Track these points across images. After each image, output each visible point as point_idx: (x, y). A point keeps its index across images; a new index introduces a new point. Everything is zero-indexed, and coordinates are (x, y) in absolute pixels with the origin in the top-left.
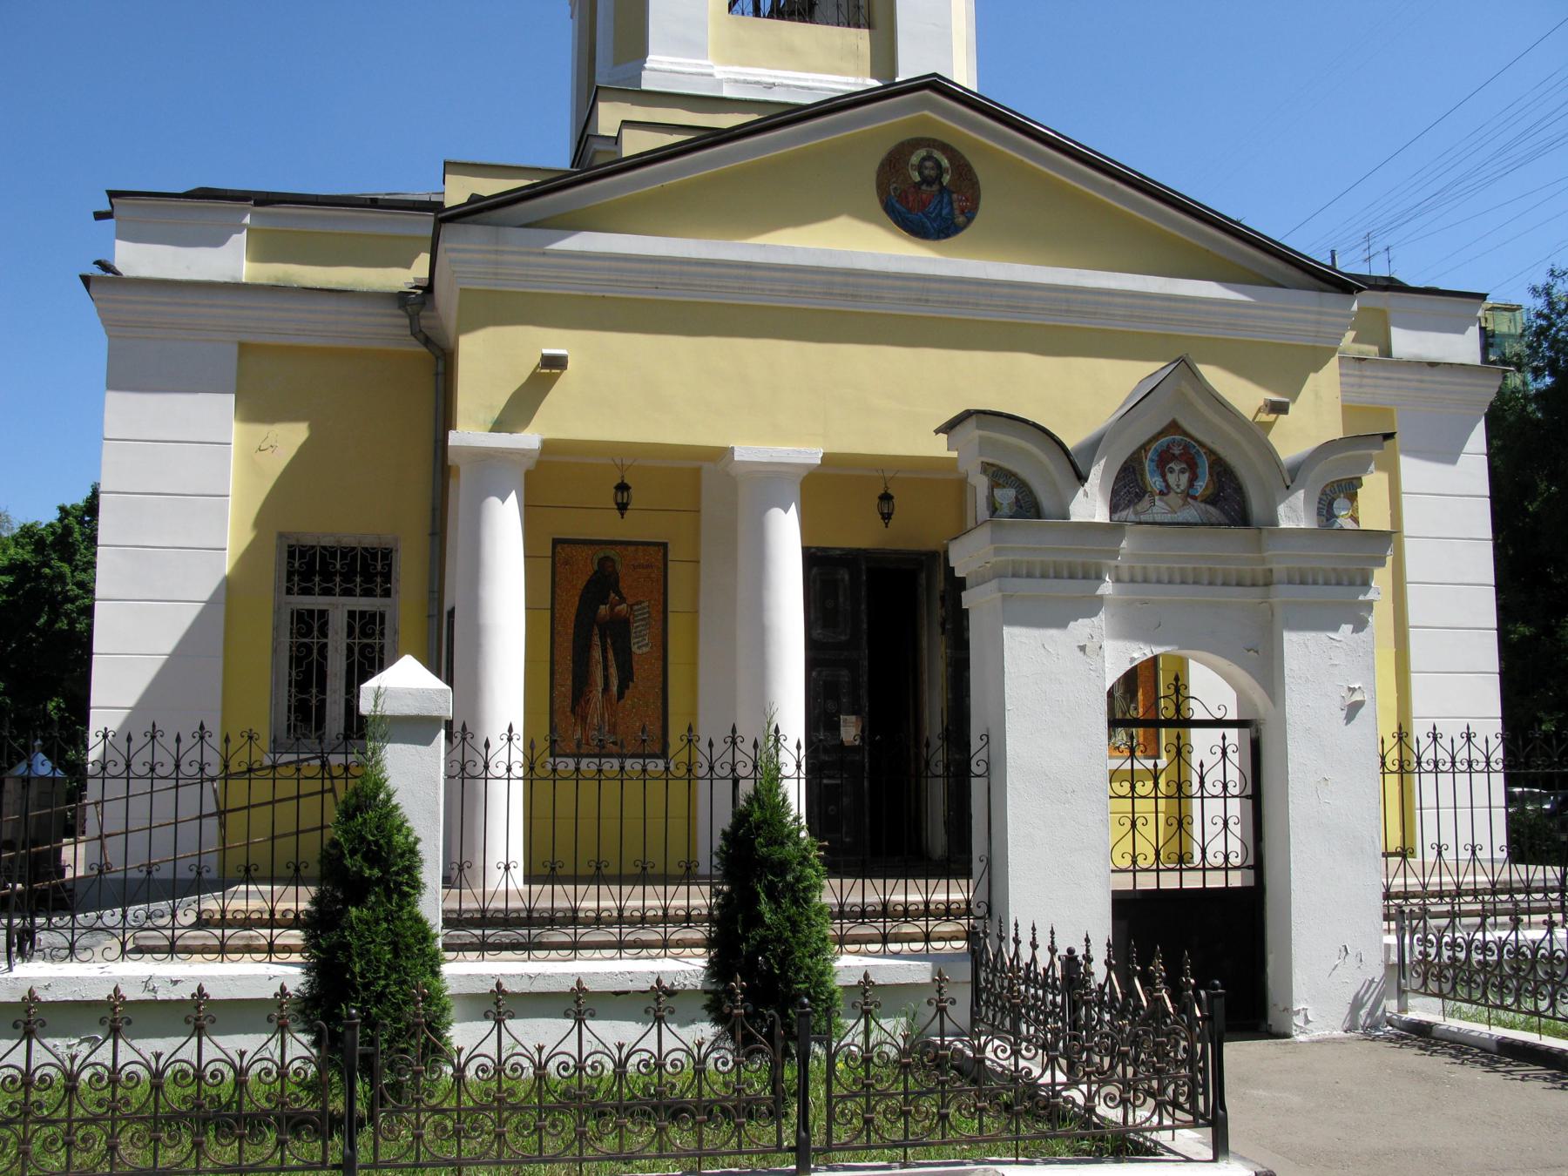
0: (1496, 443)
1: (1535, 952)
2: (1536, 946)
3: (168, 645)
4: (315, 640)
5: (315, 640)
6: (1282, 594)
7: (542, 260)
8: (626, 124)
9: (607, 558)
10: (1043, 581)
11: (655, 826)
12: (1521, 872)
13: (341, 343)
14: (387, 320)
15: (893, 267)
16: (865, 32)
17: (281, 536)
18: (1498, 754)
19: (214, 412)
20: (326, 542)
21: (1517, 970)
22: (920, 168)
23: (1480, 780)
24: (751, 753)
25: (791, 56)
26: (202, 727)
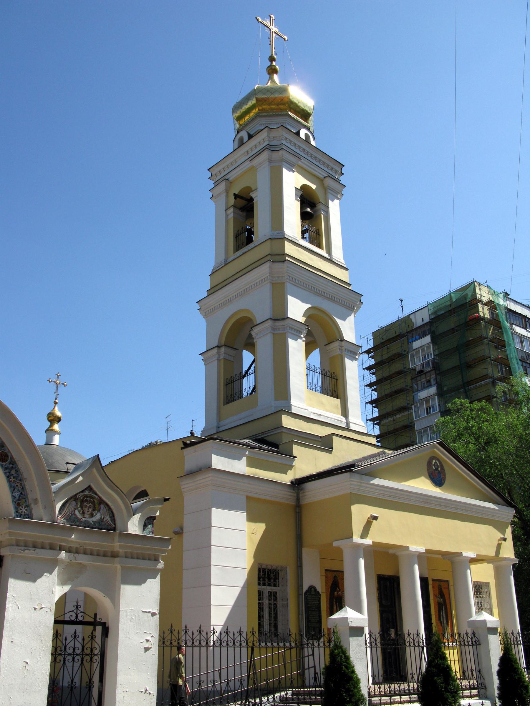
0: (517, 549)
3: (232, 602)
4: (272, 602)
7: (368, 486)
8: (333, 434)
10: (131, 560)
12: (385, 688)
13: (273, 499)
14: (290, 493)
15: (436, 495)
17: (258, 564)
18: (379, 640)
20: (269, 567)
22: (434, 465)
23: (451, 651)
25: (322, 405)
26: (75, 633)
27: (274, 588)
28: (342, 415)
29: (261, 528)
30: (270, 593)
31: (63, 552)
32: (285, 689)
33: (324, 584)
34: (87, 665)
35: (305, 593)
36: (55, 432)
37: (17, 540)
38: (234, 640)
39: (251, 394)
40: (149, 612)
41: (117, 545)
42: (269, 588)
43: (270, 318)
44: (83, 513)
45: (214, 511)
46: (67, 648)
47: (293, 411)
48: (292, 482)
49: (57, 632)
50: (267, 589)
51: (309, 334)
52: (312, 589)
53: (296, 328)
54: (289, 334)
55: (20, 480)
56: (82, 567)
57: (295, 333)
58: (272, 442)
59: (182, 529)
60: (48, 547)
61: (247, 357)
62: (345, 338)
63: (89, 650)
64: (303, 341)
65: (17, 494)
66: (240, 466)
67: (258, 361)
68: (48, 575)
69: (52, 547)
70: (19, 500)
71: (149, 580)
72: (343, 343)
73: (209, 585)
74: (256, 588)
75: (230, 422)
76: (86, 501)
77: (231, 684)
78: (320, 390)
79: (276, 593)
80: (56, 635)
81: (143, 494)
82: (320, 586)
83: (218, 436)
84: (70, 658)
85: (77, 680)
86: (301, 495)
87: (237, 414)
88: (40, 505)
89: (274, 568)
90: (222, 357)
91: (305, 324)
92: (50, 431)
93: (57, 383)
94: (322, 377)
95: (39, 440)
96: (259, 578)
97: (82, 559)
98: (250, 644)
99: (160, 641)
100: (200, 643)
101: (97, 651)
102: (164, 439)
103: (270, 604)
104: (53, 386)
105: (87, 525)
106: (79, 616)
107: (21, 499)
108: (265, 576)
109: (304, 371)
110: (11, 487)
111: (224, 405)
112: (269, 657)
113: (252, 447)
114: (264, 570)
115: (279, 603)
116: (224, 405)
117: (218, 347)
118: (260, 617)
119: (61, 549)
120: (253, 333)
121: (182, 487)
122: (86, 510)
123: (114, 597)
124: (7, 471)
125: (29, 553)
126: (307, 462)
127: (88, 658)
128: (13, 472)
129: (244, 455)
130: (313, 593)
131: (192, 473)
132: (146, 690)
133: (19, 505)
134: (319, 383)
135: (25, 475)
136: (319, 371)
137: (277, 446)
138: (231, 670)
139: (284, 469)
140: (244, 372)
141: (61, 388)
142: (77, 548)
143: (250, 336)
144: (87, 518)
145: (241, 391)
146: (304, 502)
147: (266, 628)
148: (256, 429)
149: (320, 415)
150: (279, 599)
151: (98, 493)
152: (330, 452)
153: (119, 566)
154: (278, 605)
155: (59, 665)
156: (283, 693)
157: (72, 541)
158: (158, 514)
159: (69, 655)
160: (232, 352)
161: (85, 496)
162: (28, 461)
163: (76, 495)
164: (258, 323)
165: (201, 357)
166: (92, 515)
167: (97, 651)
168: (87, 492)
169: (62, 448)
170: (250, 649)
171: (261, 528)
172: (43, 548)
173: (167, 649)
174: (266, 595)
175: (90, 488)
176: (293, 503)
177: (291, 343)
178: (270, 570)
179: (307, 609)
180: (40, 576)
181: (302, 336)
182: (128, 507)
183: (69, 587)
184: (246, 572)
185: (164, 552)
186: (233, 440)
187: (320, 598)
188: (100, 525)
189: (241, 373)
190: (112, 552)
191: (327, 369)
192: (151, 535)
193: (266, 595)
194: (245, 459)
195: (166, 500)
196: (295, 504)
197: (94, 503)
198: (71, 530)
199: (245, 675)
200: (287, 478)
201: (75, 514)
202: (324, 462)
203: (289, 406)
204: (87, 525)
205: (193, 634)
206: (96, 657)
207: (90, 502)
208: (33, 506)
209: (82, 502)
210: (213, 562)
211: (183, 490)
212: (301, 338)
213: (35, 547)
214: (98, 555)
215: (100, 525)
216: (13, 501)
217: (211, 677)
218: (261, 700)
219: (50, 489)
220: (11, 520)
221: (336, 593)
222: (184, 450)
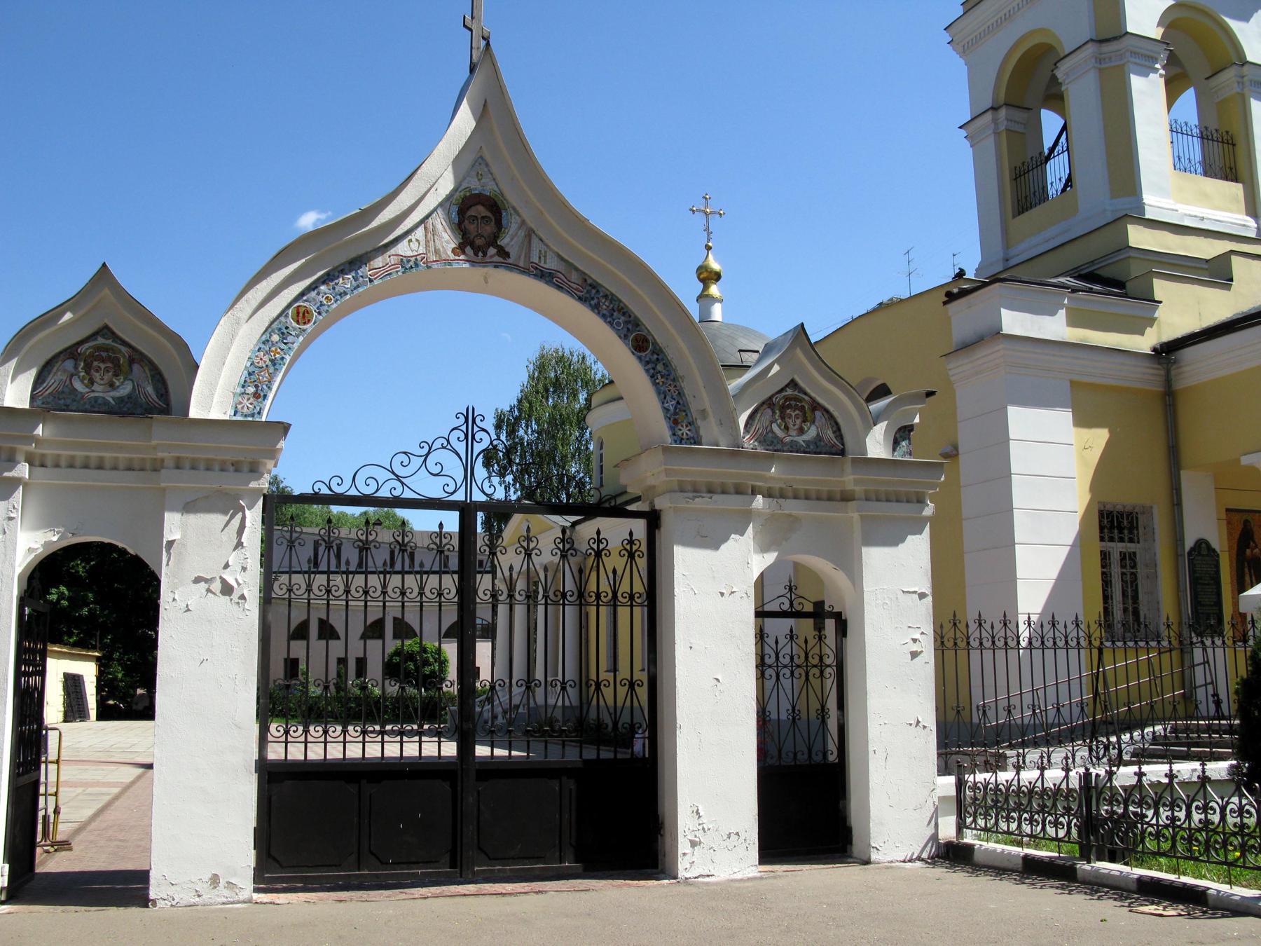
1: (985, 788)
2: (1009, 784)
3: (1054, 573)
4: (1128, 570)
5: (1128, 570)
6: (167, 479)
8: (1232, 252)
9: (178, 458)
11: (1015, 691)
14: (1152, 371)
16: (1240, 185)
19: (1060, 419)
20: (1119, 508)
21: (997, 801)
24: (774, 646)
25: (1204, 198)
27: (1129, 545)
28: (1248, 214)
29: (1099, 437)
30: (1123, 557)
31: (759, 497)
32: (1163, 720)
33: (1225, 536)
34: (815, 682)
35: (1190, 553)
36: (714, 300)
37: (680, 483)
38: (1066, 637)
39: (1064, 190)
40: (915, 592)
41: (849, 479)
42: (1120, 545)
43: (1092, 40)
44: (787, 428)
45: (1013, 411)
46: (781, 655)
47: (1149, 215)
48: (1154, 350)
49: (761, 630)
50: (1116, 548)
51: (1172, 61)
52: (1202, 547)
53: (1143, 51)
54: (1131, 66)
55: (674, 380)
56: (793, 521)
57: (1143, 62)
58: (1112, 278)
59: (956, 448)
60: (732, 490)
61: (1050, 123)
62: (1249, 58)
63: (817, 658)
64: (1161, 76)
65: (671, 405)
66: (1054, 327)
67: (1072, 127)
68: (737, 537)
69: (739, 491)
70: (675, 413)
71: (909, 537)
72: (1246, 68)
73: (1010, 544)
74: (1096, 546)
75: (1026, 248)
76: (789, 406)
77: (1065, 712)
78: (1200, 169)
79: (1135, 553)
80: (761, 636)
81: (881, 391)
82: (1218, 540)
83: (1007, 274)
84: (787, 672)
85: (801, 706)
86: (1173, 373)
87: (1040, 231)
88: (712, 419)
89: (1128, 509)
90: (1002, 128)
91: (1163, 42)
92: (704, 298)
93: (706, 213)
94: (1203, 143)
95: (694, 310)
96: (1102, 529)
97: (792, 507)
98: (1096, 643)
99: (935, 640)
100: (1006, 643)
101: (830, 660)
102: (905, 295)
103: (1123, 574)
104: (700, 218)
105: (794, 447)
106: (795, 603)
107: (678, 413)
108: (1112, 524)
109: (1164, 134)
110: (659, 393)
111: (1014, 217)
112: (1129, 668)
113: (1074, 291)
114: (1110, 514)
115: (1141, 571)
116: (1014, 217)
117: (994, 109)
118: (1106, 598)
119: (754, 492)
120: (1060, 74)
121: (951, 373)
122: (790, 423)
123: (853, 569)
124: (650, 366)
125: (702, 503)
126: (1181, 309)
127: (816, 671)
128: (660, 367)
129: (1062, 306)
130: (1204, 552)
131: (966, 347)
132: (918, 722)
133: (676, 422)
134: (1198, 157)
135: (680, 372)
136: (1196, 131)
137: (1120, 285)
138: (1063, 689)
139: (1138, 327)
140: (1046, 151)
141: (715, 222)
142: (781, 489)
143: (1054, 79)
144: (793, 436)
145: (1045, 188)
146: (1180, 385)
147: (1118, 614)
148: (1078, 256)
149: (1203, 219)
150: (1139, 566)
151: (808, 391)
152: (1227, 286)
153: (856, 516)
154: (1139, 577)
155: (770, 684)
156: (1158, 728)
157: (772, 478)
158: (917, 420)
159: (785, 666)
160: (1019, 115)
161: (787, 399)
162: (682, 345)
163: (771, 398)
164: (1067, 52)
165: (963, 133)
166: (801, 431)
167: (830, 660)
168: (789, 392)
169: (728, 326)
170: (1095, 652)
171: (1099, 437)
172: (724, 492)
173: (950, 654)
174: (1115, 557)
175: (793, 384)
176: (1159, 389)
177: (1136, 82)
178: (1121, 514)
179: (1195, 581)
180: (726, 539)
181: (1157, 66)
182: (863, 414)
183: (776, 554)
184: (1077, 518)
185: (933, 486)
186: (1039, 280)
187: (1218, 562)
188: (816, 447)
189: (1041, 153)
190: (842, 492)
191: (1212, 127)
192: (907, 458)
193: (1115, 557)
194: (1062, 313)
195: (930, 394)
196: (1161, 389)
197: (801, 410)
198: (769, 459)
199: (1088, 696)
200: (1145, 343)
201: (772, 432)
202: (1216, 306)
203: (1141, 206)
204: (794, 447)
205: (992, 627)
206: (829, 670)
207: (796, 407)
208: (699, 422)
209: (783, 408)
210: (1016, 503)
211: (952, 379)
212: (1156, 71)
213: (711, 491)
214: (818, 499)
215: (816, 447)
216: (666, 417)
217: (1027, 699)
218: (1119, 739)
219: (726, 390)
220: (666, 449)
221: (1248, 551)
222: (949, 306)
